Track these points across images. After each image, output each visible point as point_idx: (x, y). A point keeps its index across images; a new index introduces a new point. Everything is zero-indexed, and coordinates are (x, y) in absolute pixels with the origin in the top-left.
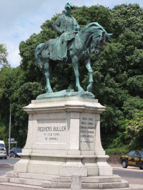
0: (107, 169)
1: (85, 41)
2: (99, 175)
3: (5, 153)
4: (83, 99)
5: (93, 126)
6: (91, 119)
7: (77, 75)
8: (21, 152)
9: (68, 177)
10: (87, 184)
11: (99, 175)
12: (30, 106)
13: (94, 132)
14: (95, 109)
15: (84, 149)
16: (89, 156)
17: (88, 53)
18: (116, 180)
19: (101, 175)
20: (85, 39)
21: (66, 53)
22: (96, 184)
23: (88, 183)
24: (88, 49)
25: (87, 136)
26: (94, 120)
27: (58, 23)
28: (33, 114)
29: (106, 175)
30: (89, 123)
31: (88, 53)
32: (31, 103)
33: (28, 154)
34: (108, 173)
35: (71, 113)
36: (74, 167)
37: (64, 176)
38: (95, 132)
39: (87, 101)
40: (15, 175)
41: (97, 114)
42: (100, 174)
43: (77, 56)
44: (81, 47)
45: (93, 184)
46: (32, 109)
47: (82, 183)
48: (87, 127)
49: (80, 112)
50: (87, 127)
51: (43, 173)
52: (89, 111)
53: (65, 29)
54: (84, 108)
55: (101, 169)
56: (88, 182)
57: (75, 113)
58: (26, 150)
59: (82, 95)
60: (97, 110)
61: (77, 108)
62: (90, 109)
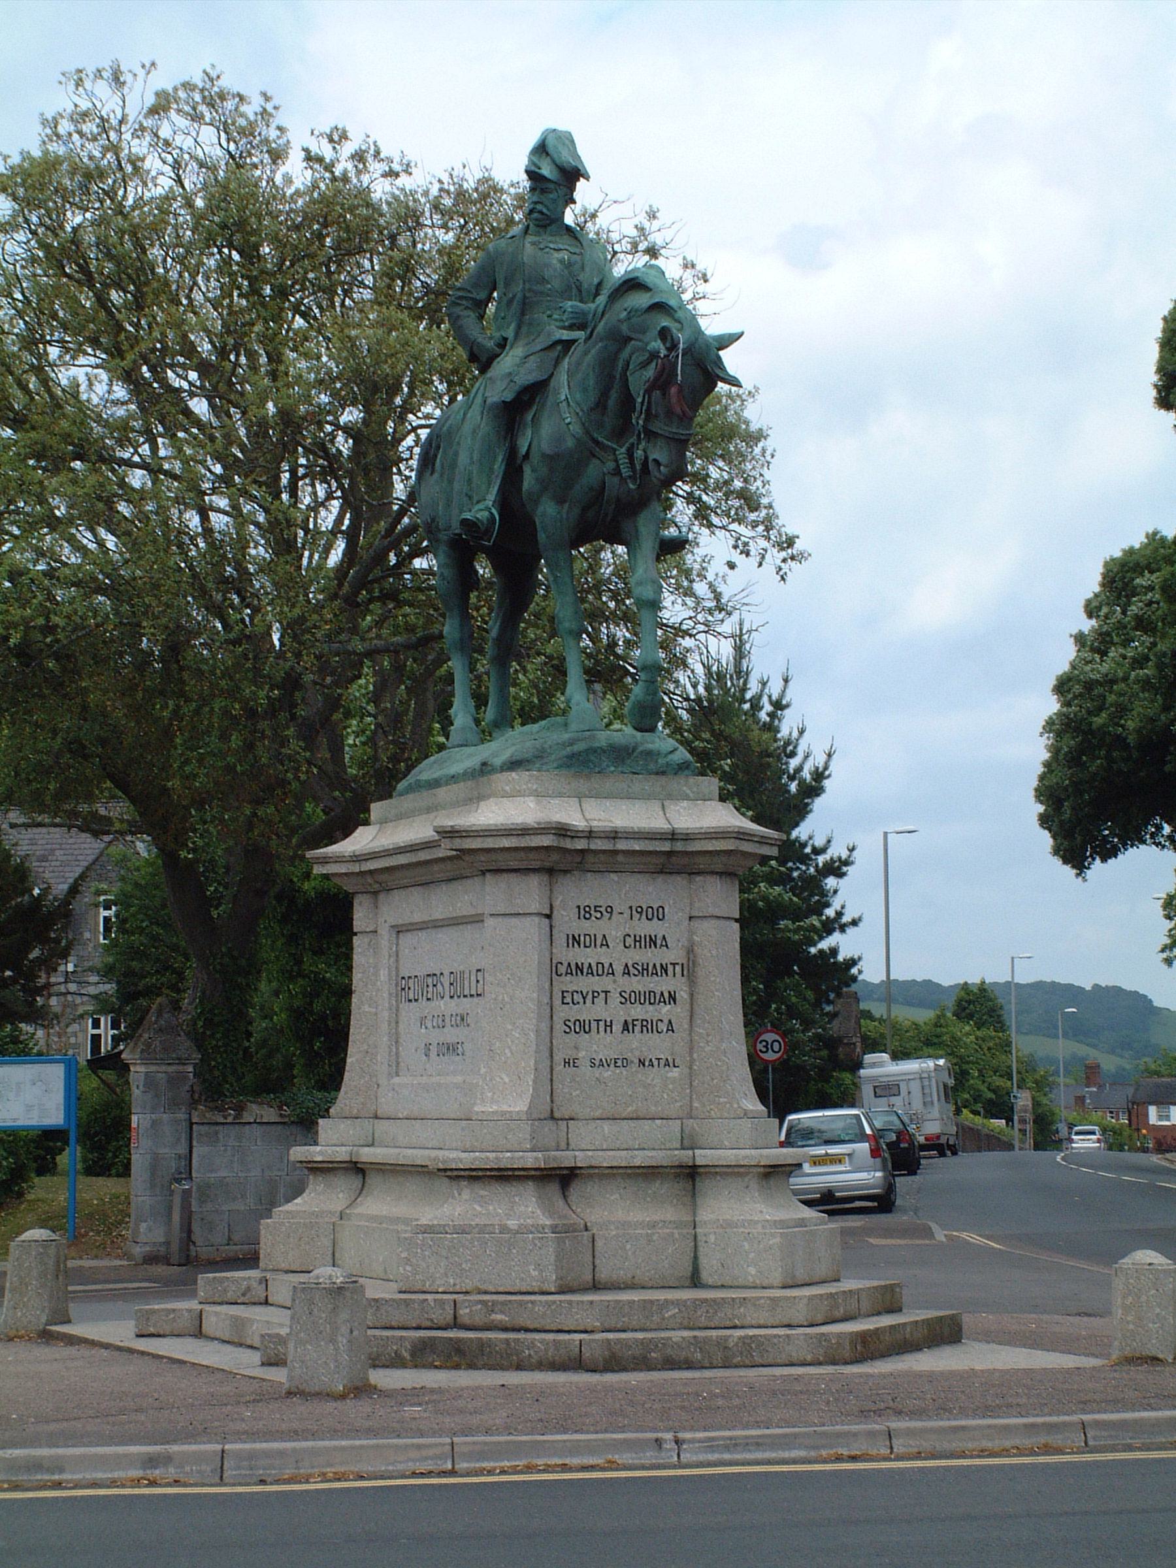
0: (746, 1246)
1: (593, 397)
2: (695, 1281)
3: (1099, 1141)
4: (582, 785)
5: (674, 954)
6: (658, 914)
7: (567, 625)
8: (316, 1143)
9: (422, 1297)
10: (512, 1336)
11: (695, 1281)
12: (361, 840)
13: (683, 995)
14: (666, 847)
15: (598, 1114)
16: (492, 1155)
17: (625, 471)
18: (763, 1317)
19: (710, 1282)
20: (592, 382)
21: (494, 490)
22: (566, 1337)
23: (521, 1336)
24: (623, 450)
25: (617, 1027)
26: (675, 914)
27: (476, 285)
28: (375, 893)
29: (741, 1282)
30: (629, 941)
31: (625, 471)
32: (366, 823)
33: (342, 1154)
34: (752, 1270)
35: (488, 875)
36: (482, 1229)
37: (418, 1287)
38: (692, 995)
39: (609, 796)
40: (248, 1289)
41: (699, 873)
42: (705, 1276)
43: (560, 501)
44: (570, 443)
45: (550, 1337)
46: (356, 858)
47: (370, 1332)
48: (619, 968)
49: (551, 871)
50: (619, 968)
51: (386, 1272)
52: (620, 858)
53: (513, 326)
54: (546, 841)
55: (712, 1238)
56: (537, 1326)
57: (513, 878)
58: (343, 1125)
59: (572, 756)
60: (679, 846)
61: (506, 843)
62: (621, 845)
